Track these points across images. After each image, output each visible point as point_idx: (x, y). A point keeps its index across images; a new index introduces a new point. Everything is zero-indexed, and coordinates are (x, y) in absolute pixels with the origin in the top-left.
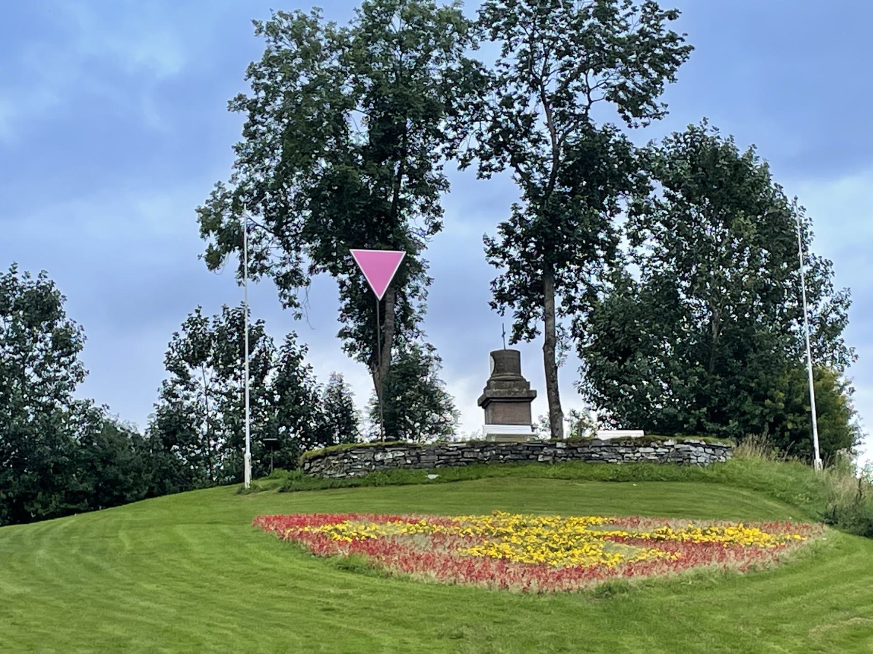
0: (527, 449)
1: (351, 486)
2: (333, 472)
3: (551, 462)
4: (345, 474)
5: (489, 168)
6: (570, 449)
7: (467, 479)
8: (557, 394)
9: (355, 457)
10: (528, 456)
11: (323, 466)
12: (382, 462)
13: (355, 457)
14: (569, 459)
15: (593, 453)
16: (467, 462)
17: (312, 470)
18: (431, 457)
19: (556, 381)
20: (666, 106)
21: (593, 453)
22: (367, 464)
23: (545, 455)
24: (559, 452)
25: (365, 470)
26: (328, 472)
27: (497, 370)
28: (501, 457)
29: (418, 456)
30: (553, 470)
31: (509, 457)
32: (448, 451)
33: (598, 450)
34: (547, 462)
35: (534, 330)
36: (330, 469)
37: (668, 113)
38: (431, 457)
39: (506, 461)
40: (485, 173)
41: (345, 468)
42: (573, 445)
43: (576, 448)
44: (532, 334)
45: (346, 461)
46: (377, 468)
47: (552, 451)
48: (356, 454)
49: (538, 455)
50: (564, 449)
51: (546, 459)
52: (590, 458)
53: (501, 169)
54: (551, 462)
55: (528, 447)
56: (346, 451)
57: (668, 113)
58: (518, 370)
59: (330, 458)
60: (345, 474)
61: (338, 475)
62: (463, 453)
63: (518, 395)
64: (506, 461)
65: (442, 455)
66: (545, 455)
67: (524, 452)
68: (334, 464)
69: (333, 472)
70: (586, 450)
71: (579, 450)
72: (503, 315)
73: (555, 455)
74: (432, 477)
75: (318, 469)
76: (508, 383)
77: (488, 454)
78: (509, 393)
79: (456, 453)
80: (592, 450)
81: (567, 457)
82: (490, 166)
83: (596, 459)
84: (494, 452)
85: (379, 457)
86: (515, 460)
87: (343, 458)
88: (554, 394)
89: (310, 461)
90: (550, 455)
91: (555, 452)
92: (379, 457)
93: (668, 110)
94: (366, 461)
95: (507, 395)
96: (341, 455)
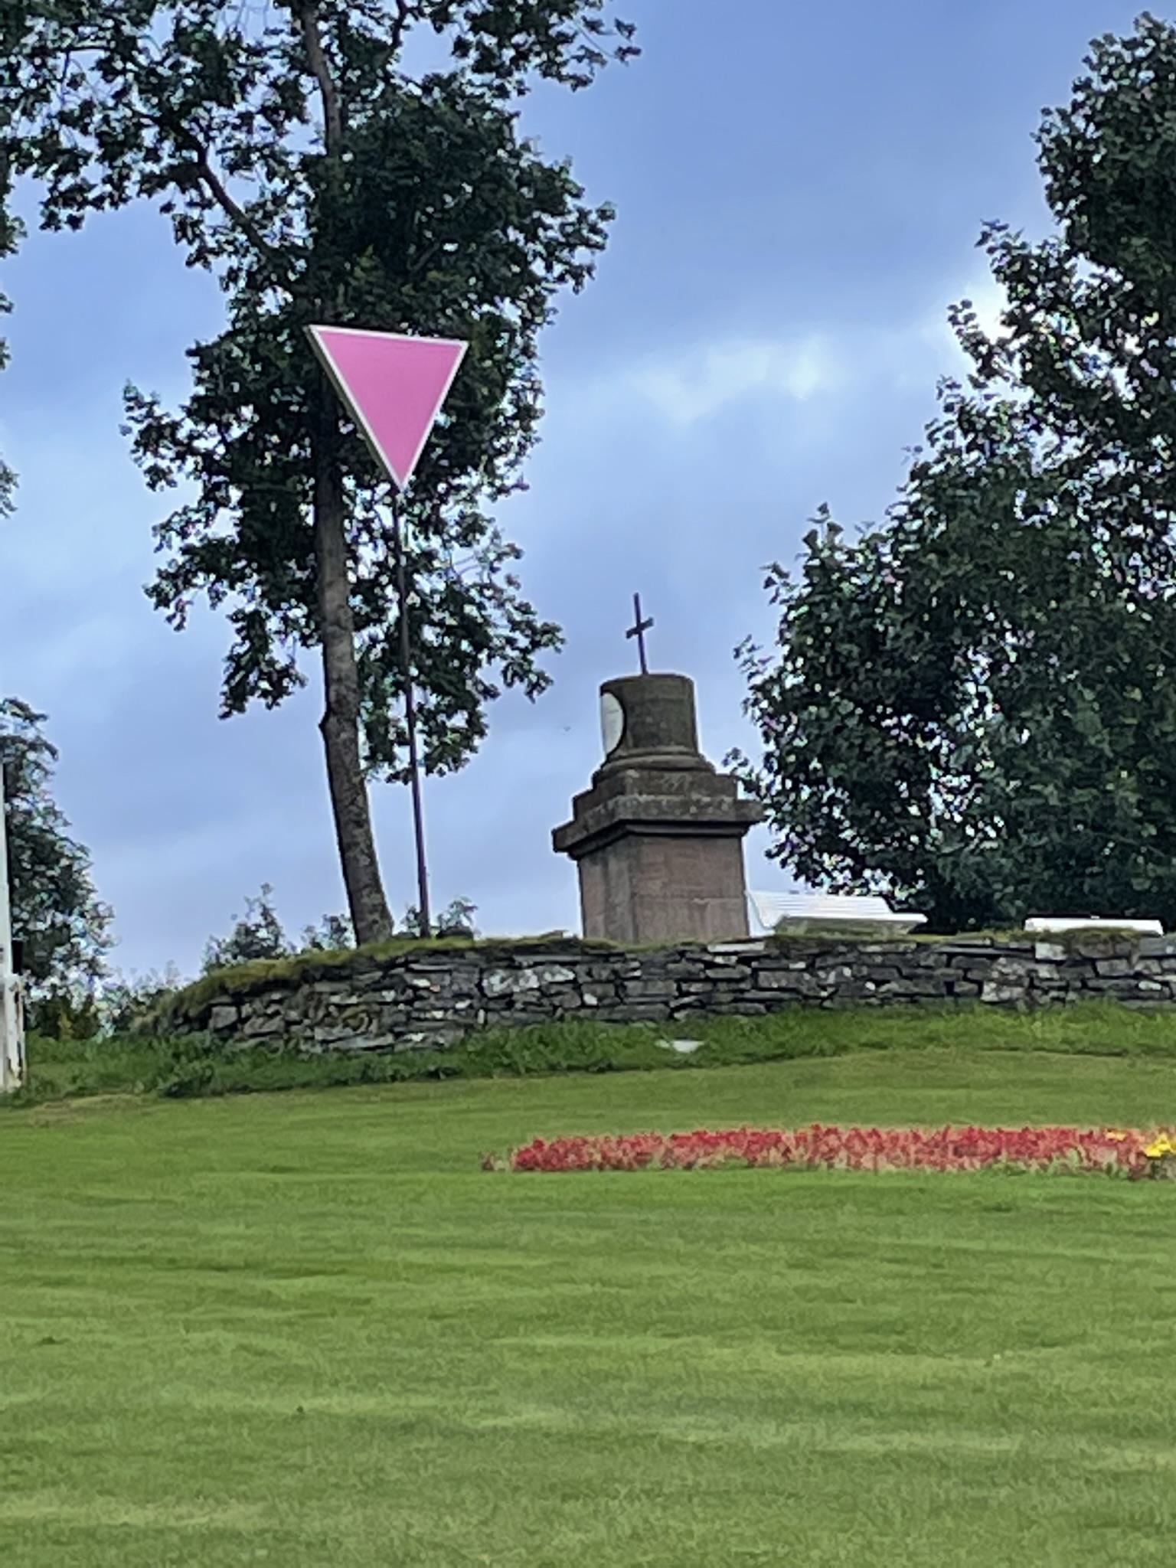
0: (948, 965)
1: (434, 1075)
2: (337, 1032)
3: (1021, 1006)
4: (389, 1039)
5: (75, 197)
6: (1075, 964)
7: (808, 1053)
8: (373, 862)
9: (423, 983)
10: (950, 986)
11: (294, 1015)
12: (507, 999)
13: (423, 983)
14: (1072, 996)
15: (1139, 976)
16: (770, 1005)
17: (248, 1029)
18: (659, 987)
19: (367, 821)
20: (630, 30)
21: (1139, 976)
22: (461, 1005)
23: (1003, 982)
24: (1044, 972)
25: (458, 1025)
26: (319, 1034)
27: (633, 735)
28: (871, 986)
29: (618, 981)
30: (1043, 1028)
31: (894, 986)
32: (710, 965)
33: (1155, 967)
34: (1008, 1005)
35: (285, 672)
36: (328, 1021)
37: (636, 52)
38: (659, 987)
39: (885, 1001)
40: (64, 214)
41: (387, 1020)
42: (1084, 951)
43: (1093, 962)
44: (280, 681)
45: (389, 996)
46: (493, 1018)
47: (1019, 968)
48: (421, 974)
49: (980, 984)
50: (1058, 963)
51: (1006, 994)
52: (1134, 994)
53: (118, 199)
54: (1021, 1006)
55: (951, 956)
56: (392, 964)
57: (636, 52)
58: (694, 744)
59: (322, 987)
60: (389, 1039)
61: (360, 1042)
62: (755, 971)
63: (710, 815)
64: (885, 1001)
65: (690, 978)
66: (1003, 982)
67: (938, 972)
68: (341, 1008)
69: (337, 1032)
70: (1122, 966)
71: (1102, 967)
72: (179, 627)
73: (1032, 983)
74: (684, 1047)
75: (276, 1024)
76: (677, 775)
77: (832, 978)
78: (685, 805)
79: (735, 974)
80: (1139, 968)
81: (1065, 989)
82: (82, 188)
83: (1150, 995)
84: (847, 972)
85: (496, 983)
86: (912, 998)
87: (377, 987)
88: (364, 861)
89: (238, 1000)
90: (1018, 983)
91: (1031, 974)
92: (496, 983)
93: (634, 42)
94: (459, 996)
95: (677, 815)
96: (366, 978)
